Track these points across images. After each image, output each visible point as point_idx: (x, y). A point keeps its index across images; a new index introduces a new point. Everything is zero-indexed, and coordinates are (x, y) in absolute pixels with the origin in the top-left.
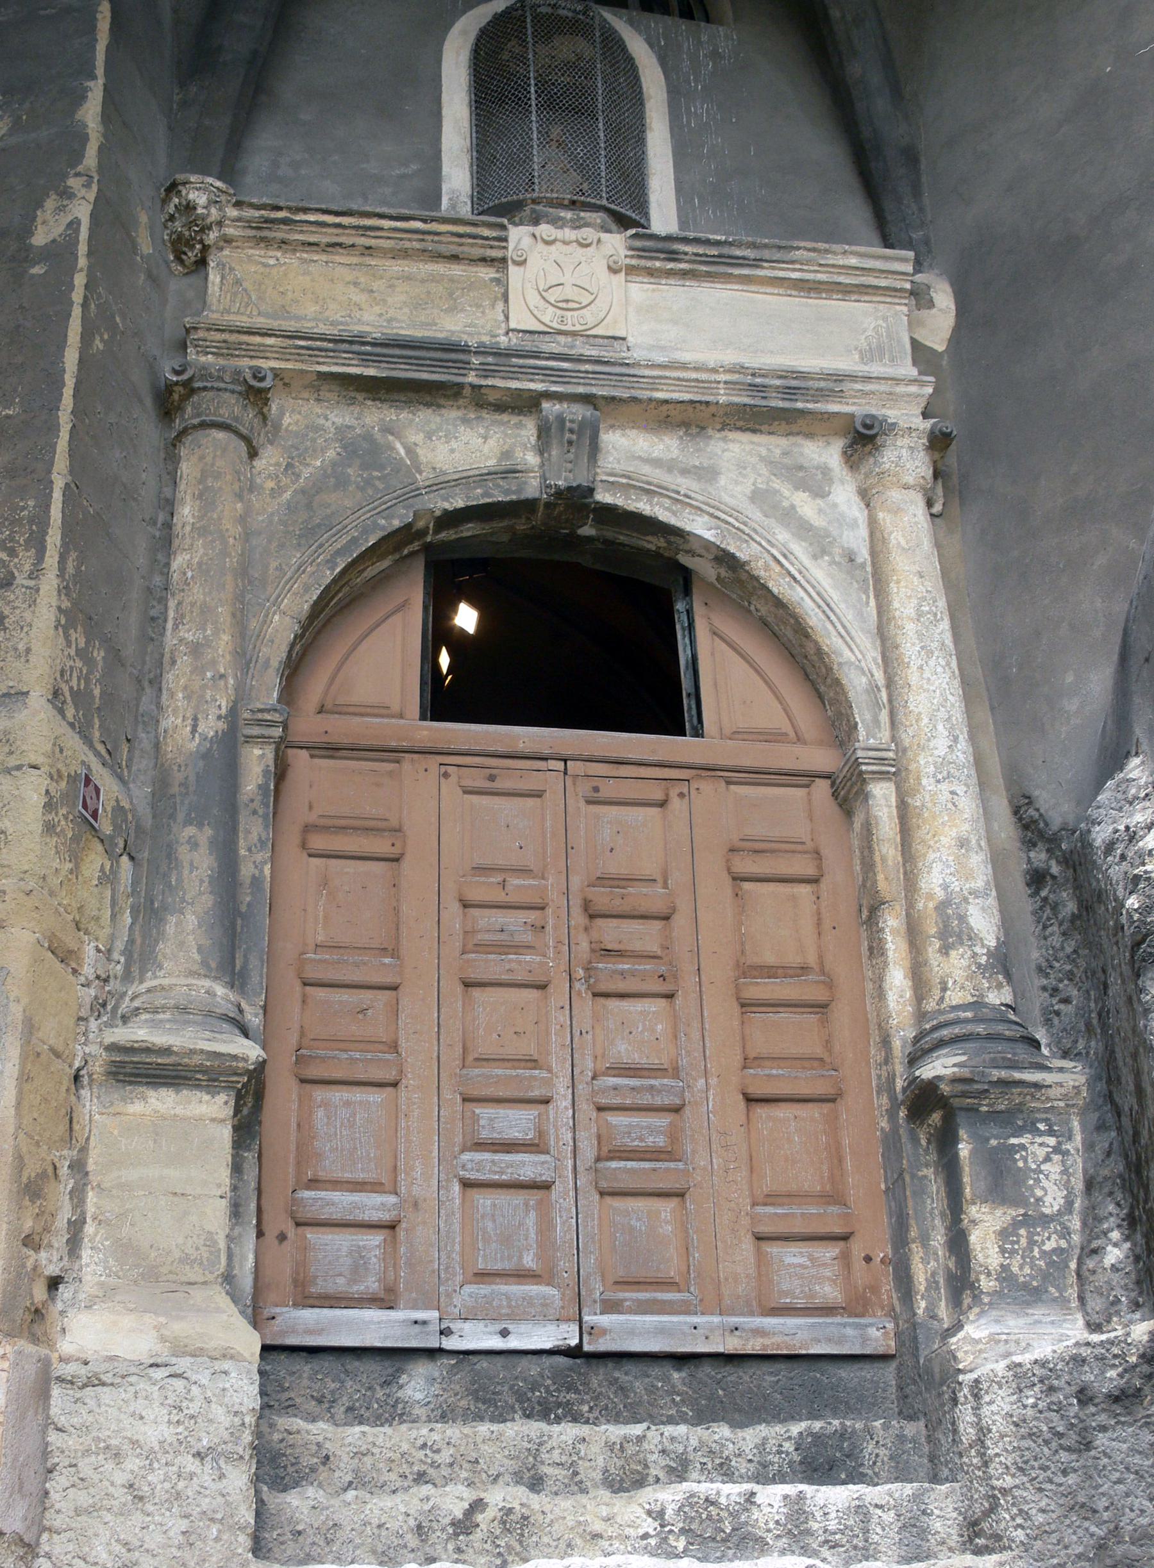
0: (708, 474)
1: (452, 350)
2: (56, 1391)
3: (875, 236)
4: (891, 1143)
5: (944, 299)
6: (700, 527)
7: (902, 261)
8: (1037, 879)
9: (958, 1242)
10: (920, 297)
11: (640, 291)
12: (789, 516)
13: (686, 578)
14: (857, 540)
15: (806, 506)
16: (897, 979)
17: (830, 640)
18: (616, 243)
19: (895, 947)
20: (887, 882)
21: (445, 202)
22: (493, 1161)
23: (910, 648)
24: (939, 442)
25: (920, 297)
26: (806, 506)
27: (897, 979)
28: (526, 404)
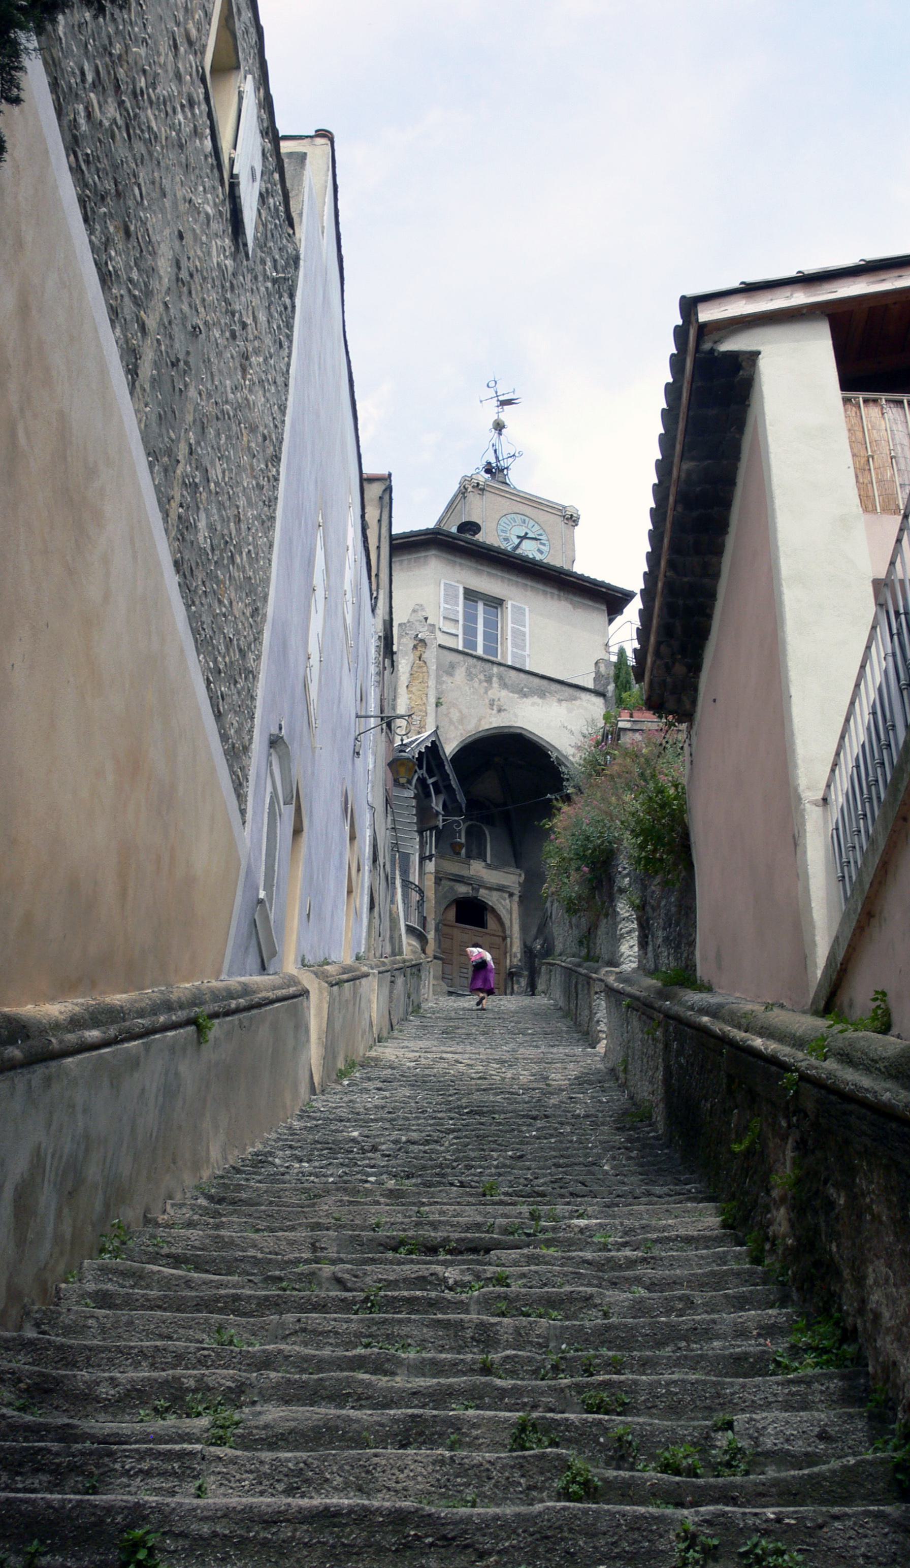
0: (491, 896)
1: (463, 877)
2: (404, 742)
3: (513, 863)
4: (506, 979)
5: (523, 876)
6: (490, 903)
7: (518, 871)
8: (525, 952)
9: (513, 988)
10: (520, 875)
11: (485, 870)
12: (501, 903)
13: (486, 909)
14: (509, 907)
15: (503, 902)
16: (508, 961)
17: (504, 919)
18: (483, 864)
19: (508, 957)
20: (508, 950)
21: (699, 982)
22: (626, 1423)
23: (514, 921)
24: (520, 897)
25: (520, 875)
26: (503, 902)
27: (508, 961)
28: (471, 884)
